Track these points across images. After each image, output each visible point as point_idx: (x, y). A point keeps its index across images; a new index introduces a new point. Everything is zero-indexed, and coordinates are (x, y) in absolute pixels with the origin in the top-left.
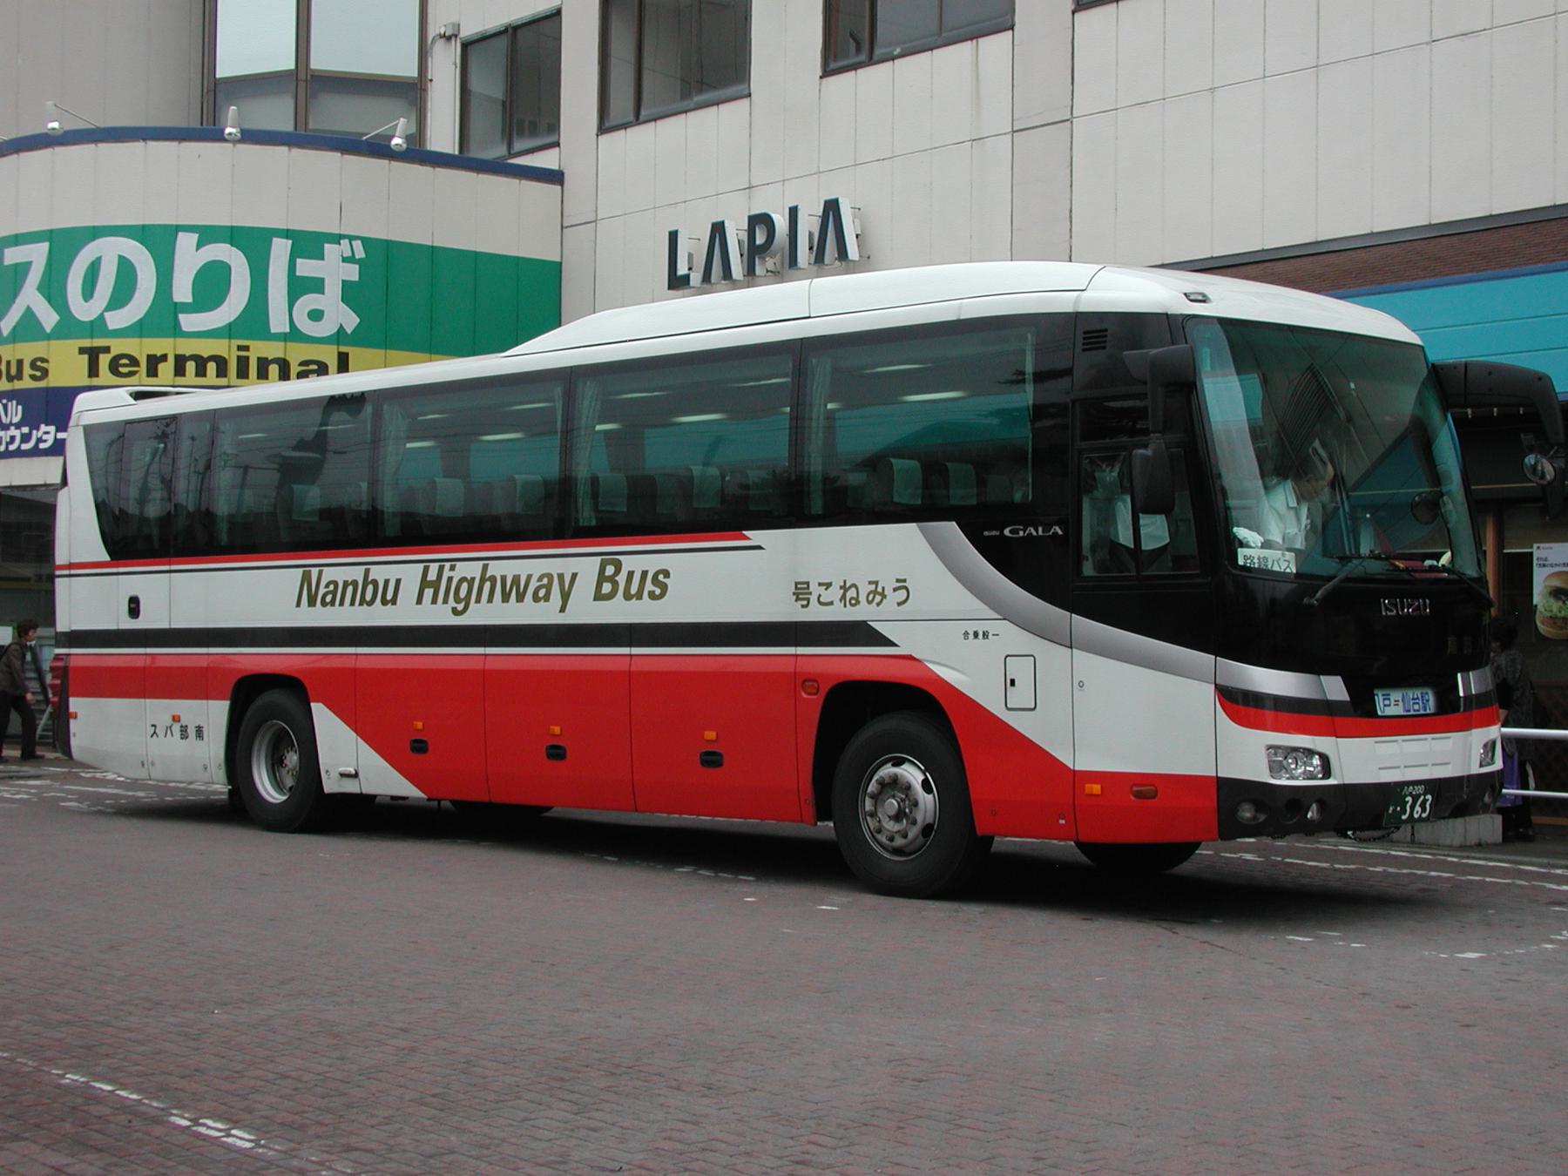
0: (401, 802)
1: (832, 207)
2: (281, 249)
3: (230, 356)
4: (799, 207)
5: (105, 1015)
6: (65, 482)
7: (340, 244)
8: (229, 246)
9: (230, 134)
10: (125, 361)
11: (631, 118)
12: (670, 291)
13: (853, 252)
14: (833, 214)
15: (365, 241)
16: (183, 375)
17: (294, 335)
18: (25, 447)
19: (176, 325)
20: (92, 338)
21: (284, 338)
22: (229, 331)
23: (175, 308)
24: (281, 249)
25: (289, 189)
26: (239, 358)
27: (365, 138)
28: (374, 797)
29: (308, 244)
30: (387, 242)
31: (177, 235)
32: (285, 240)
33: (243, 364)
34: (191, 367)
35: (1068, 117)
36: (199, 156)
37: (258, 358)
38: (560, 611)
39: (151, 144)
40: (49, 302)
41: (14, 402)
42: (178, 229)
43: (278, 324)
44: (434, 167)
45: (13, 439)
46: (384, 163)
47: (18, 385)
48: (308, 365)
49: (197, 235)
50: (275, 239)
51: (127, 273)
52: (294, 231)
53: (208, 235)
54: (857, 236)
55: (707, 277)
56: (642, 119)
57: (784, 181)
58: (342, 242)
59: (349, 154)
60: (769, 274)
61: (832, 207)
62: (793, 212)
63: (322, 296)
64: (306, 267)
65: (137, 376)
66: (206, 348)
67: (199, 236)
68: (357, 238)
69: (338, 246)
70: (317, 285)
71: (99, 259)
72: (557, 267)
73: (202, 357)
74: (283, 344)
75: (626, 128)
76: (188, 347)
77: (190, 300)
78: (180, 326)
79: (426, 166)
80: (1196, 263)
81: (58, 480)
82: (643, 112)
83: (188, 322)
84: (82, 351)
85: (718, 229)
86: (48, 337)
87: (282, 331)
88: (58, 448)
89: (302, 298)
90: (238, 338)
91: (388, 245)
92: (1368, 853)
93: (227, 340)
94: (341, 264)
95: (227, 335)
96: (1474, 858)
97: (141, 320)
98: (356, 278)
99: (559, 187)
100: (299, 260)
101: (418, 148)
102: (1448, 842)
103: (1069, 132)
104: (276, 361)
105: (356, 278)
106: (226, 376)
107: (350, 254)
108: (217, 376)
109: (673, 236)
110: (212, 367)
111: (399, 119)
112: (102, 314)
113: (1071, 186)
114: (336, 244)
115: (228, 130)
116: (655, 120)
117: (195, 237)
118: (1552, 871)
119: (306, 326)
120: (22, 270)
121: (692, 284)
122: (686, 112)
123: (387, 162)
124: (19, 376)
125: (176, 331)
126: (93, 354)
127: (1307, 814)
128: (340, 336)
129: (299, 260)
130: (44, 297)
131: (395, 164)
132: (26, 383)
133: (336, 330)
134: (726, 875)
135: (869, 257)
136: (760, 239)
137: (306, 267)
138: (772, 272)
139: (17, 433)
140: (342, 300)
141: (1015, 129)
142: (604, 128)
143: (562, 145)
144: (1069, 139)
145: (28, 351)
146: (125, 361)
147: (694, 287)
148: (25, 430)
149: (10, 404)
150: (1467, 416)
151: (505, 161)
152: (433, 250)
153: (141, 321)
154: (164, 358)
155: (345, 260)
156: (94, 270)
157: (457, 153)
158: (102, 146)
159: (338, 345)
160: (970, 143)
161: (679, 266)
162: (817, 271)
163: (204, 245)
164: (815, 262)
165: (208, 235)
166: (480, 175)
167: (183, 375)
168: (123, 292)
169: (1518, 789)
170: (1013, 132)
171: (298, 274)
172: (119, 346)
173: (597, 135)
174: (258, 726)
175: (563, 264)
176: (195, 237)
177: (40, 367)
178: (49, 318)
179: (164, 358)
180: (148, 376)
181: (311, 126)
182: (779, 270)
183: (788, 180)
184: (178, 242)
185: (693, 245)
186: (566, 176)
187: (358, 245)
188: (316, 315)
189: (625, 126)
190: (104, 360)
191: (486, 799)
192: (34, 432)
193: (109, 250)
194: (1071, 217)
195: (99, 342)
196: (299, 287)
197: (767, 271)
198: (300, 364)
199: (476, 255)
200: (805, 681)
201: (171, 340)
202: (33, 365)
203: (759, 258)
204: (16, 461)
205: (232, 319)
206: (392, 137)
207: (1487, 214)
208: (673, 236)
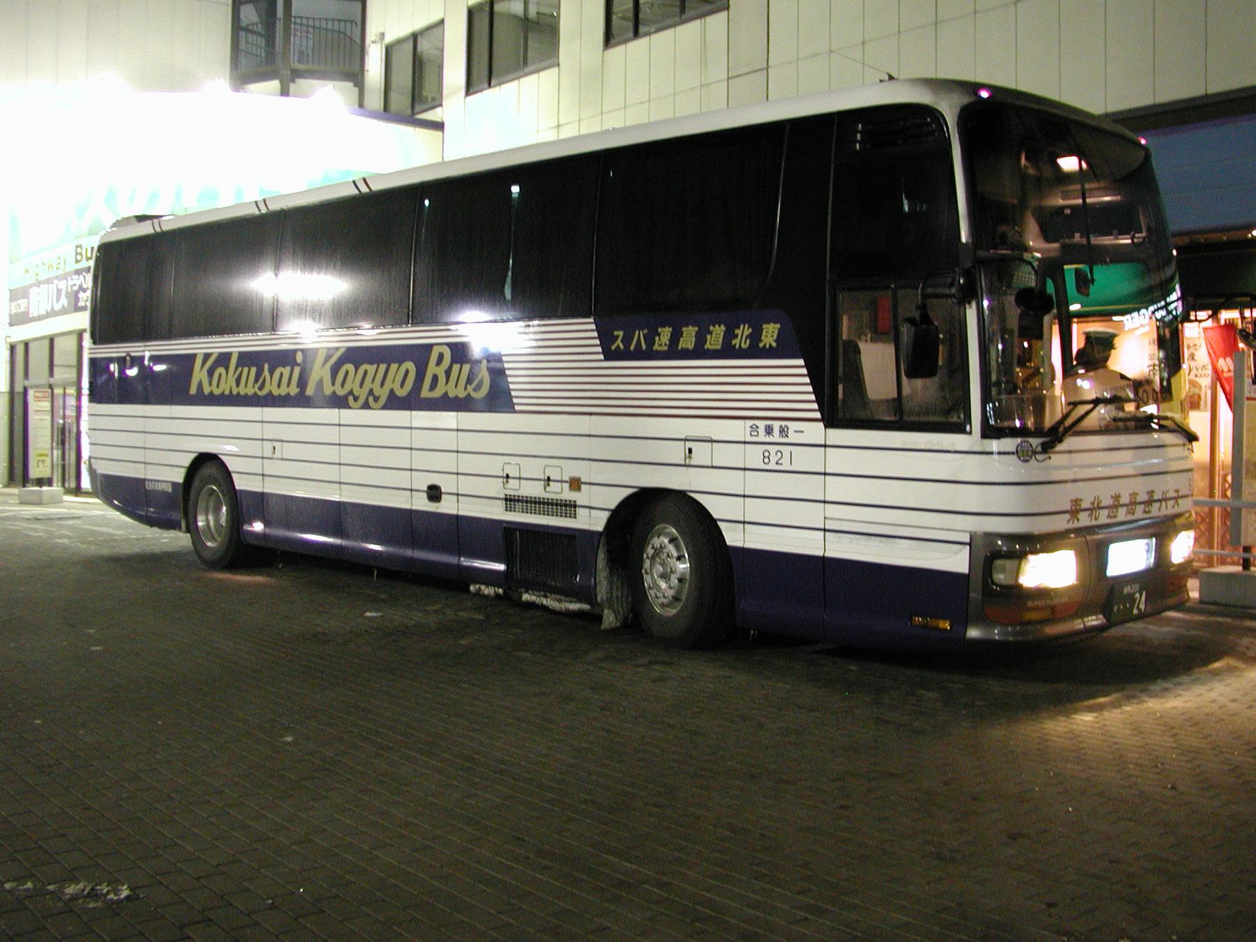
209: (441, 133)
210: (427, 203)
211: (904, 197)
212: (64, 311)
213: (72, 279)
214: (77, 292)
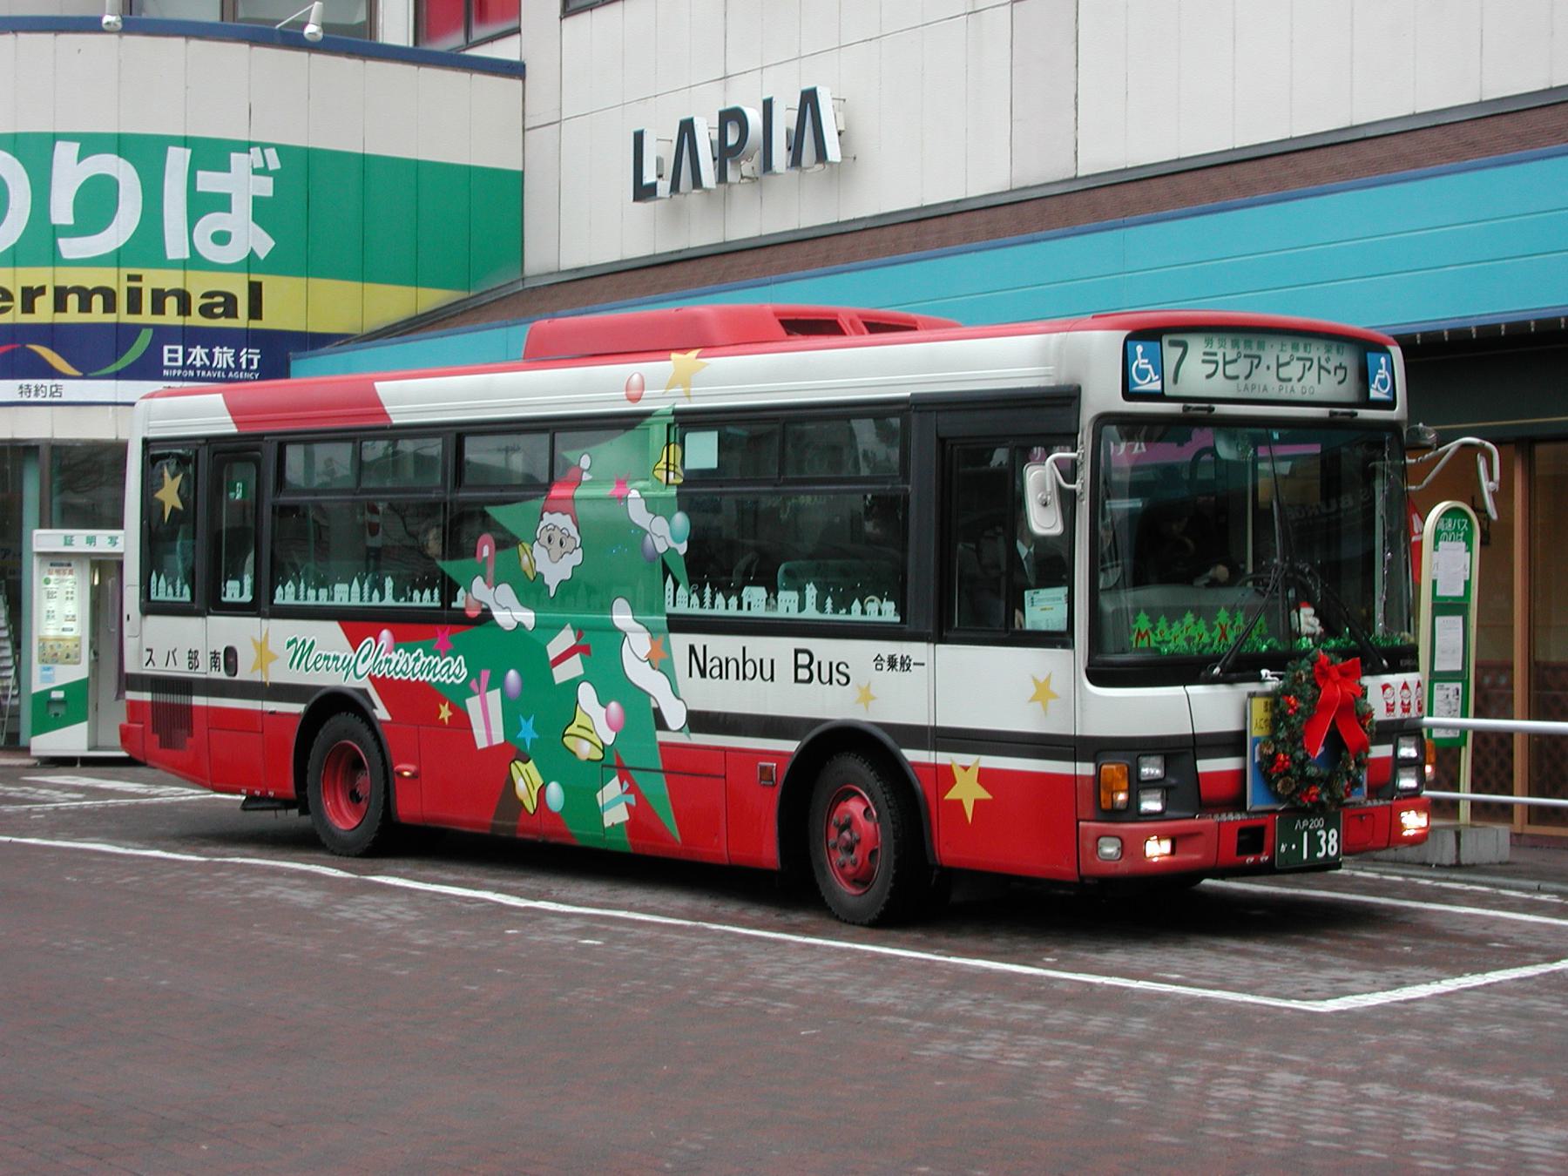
1: (809, 99)
2: (178, 159)
3: (118, 288)
5: (1292, 1111)
7: (249, 153)
8: (115, 157)
9: (108, 23)
13: (833, 152)
15: (282, 150)
16: (65, 310)
17: (195, 262)
19: (54, 249)
21: (184, 265)
22: (117, 258)
24: (178, 159)
25: (187, 88)
26: (130, 290)
27: (278, 26)
30: (308, 150)
34: (73, 300)
36: (79, 51)
39: (22, 36)
42: (56, 137)
43: (176, 247)
44: (364, 60)
46: (304, 55)
48: (213, 298)
52: (192, 138)
53: (90, 144)
54: (839, 134)
55: (675, 187)
57: (762, 68)
58: (251, 150)
60: (745, 180)
61: (809, 99)
62: (768, 106)
63: (228, 215)
64: (209, 182)
65: (11, 311)
66: (91, 279)
67: (81, 146)
68: (270, 146)
69: (246, 155)
70: (222, 203)
76: (69, 278)
77: (71, 222)
78: (60, 254)
79: (355, 58)
80: (1216, 156)
83: (70, 248)
85: (687, 128)
87: (181, 257)
89: (204, 218)
91: (309, 155)
93: (115, 269)
94: (252, 177)
95: (115, 262)
96: (1455, 881)
97: (14, 246)
98: (270, 194)
99: (519, 82)
100: (200, 174)
101: (368, 41)
102: (1436, 860)
104: (174, 292)
105: (270, 194)
107: (262, 165)
109: (639, 138)
110: (97, 301)
111: (313, 3)
113: (1077, 65)
114: (245, 152)
115: (107, 19)
117: (76, 146)
118: (1536, 897)
121: (659, 194)
125: (55, 259)
128: (251, 263)
129: (200, 174)
136: (732, 139)
137: (209, 182)
138: (749, 178)
140: (253, 220)
144: (1075, 9)
146: (219, 310)
147: (660, 198)
151: (462, 53)
152: (364, 157)
153: (118, 251)
155: (256, 172)
157: (411, 45)
159: (249, 272)
161: (645, 174)
162: (799, 176)
164: (792, 165)
165: (90, 144)
166: (421, 69)
167: (65, 310)
169: (1523, 795)
171: (199, 189)
175: (526, 174)
176: (76, 146)
181: (241, 14)
182: (758, 175)
185: (660, 149)
187: (271, 154)
188: (222, 238)
194: (1076, 104)
196: (200, 204)
197: (742, 177)
198: (205, 296)
199: (418, 165)
201: (49, 270)
203: (731, 162)
205: (121, 244)
206: (305, 24)
207: (1547, 87)
208: (639, 138)
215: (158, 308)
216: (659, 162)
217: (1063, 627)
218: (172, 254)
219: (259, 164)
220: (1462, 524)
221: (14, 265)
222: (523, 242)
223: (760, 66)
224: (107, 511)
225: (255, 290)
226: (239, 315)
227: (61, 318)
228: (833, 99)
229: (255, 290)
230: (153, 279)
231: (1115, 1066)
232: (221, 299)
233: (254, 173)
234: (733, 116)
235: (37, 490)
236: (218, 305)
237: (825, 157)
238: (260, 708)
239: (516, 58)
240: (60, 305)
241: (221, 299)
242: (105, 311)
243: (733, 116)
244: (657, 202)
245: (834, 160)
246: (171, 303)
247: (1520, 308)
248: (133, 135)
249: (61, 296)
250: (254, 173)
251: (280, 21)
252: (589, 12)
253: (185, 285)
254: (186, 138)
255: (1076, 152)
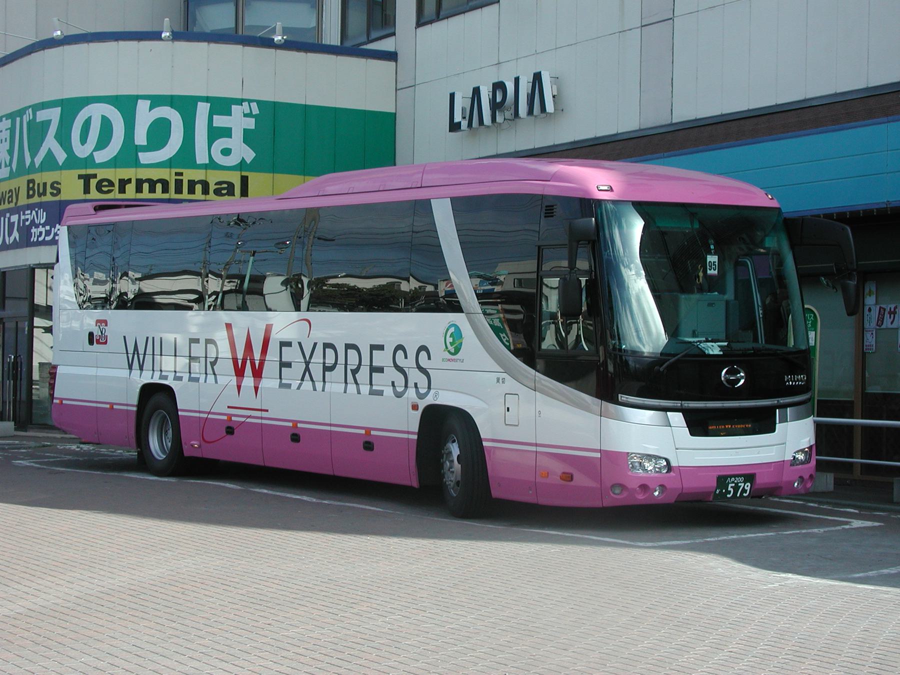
0: (844, 576)
1: (537, 77)
2: (203, 109)
4: (520, 77)
6: (58, 261)
7: (242, 105)
8: (170, 108)
10: (105, 183)
11: (434, 17)
12: (450, 133)
13: (550, 107)
14: (538, 82)
15: (259, 102)
17: (212, 165)
18: (48, 238)
20: (86, 168)
21: (205, 167)
22: (169, 163)
23: (136, 149)
24: (203, 109)
28: (219, 460)
29: (221, 106)
31: (137, 101)
32: (205, 104)
33: (179, 184)
34: (146, 186)
35: (672, 16)
37: (189, 180)
38: (317, 343)
40: (61, 146)
41: (42, 210)
43: (202, 158)
44: (306, 53)
45: (41, 233)
47: (44, 199)
48: (221, 185)
49: (150, 101)
50: (199, 103)
51: (107, 126)
53: (156, 101)
54: (554, 97)
56: (441, 17)
57: (517, 59)
58: (243, 104)
59: (248, 46)
61: (537, 77)
62: (517, 80)
63: (230, 139)
64: (220, 121)
65: (113, 192)
66: (155, 174)
69: (240, 106)
70: (227, 132)
71: (90, 118)
72: (393, 117)
73: (153, 180)
74: (204, 171)
75: (431, 23)
76: (144, 174)
79: (301, 52)
81: (54, 261)
82: (442, 13)
83: (145, 158)
84: (80, 177)
85: (476, 91)
86: (61, 168)
87: (204, 163)
88: (54, 242)
90: (176, 168)
91: (275, 104)
92: (841, 511)
97: (115, 157)
99: (394, 63)
103: (672, 26)
104: (200, 182)
106: (168, 193)
107: (249, 112)
108: (163, 193)
109: (452, 96)
110: (159, 187)
112: (92, 153)
114: (239, 105)
116: (447, 18)
119: (220, 159)
120: (47, 124)
122: (464, 13)
123: (274, 50)
124: (44, 193)
125: (137, 164)
126: (87, 179)
127: (794, 485)
128: (242, 165)
130: (58, 142)
131: (279, 51)
132: (48, 198)
133: (240, 161)
134: (398, 513)
135: (562, 110)
137: (220, 121)
139: (43, 230)
140: (244, 142)
141: (642, 25)
142: (420, 24)
143: (396, 35)
145: (48, 177)
146: (224, 192)
147: (463, 130)
148: (48, 228)
149: (39, 211)
150: (847, 216)
152: (306, 107)
154: (129, 181)
155: (245, 115)
156: (87, 124)
158: (92, 45)
160: (618, 34)
161: (455, 117)
163: (152, 109)
168: (104, 140)
170: (642, 26)
172: (102, 174)
173: (416, 28)
174: (150, 418)
177: (56, 188)
178: (61, 156)
179: (129, 181)
180: (119, 193)
183: (519, 58)
184: (137, 107)
186: (398, 55)
187: (254, 106)
188: (226, 152)
189: (431, 22)
190: (93, 182)
191: (262, 464)
192: (53, 229)
193: (96, 111)
194: (672, 83)
195: (90, 171)
196: (215, 133)
197: (505, 119)
198: (216, 184)
200: (506, 394)
201: (134, 169)
202: (52, 187)
203: (499, 112)
204: (43, 248)
209: (393, 64)
210: (735, 367)
211: (738, 385)
212: (15, 245)
213: (24, 214)
214: (30, 227)
215: (192, 191)
216: (463, 110)
217: (283, 348)
218: (199, 161)
219: (247, 111)
220: (810, 317)
221: (115, 167)
222: (395, 155)
223: (516, 58)
224: (479, 298)
225: (244, 181)
226: (235, 194)
227: (140, 196)
228: (551, 77)
229: (244, 181)
230: (189, 175)
231: (534, 569)
232: (226, 186)
233: (244, 116)
234: (499, 86)
235: (792, 256)
236: (224, 189)
237: (472, 126)
238: (332, 427)
239: (392, 50)
240: (139, 189)
241: (226, 186)
242: (163, 192)
243: (499, 86)
244: (461, 133)
245: (499, 122)
246: (199, 188)
247: (840, 205)
248: (176, 95)
249: (139, 184)
250: (244, 116)
251: (270, 27)
252: (430, 25)
253: (206, 177)
254: (207, 97)
255: (672, 110)
